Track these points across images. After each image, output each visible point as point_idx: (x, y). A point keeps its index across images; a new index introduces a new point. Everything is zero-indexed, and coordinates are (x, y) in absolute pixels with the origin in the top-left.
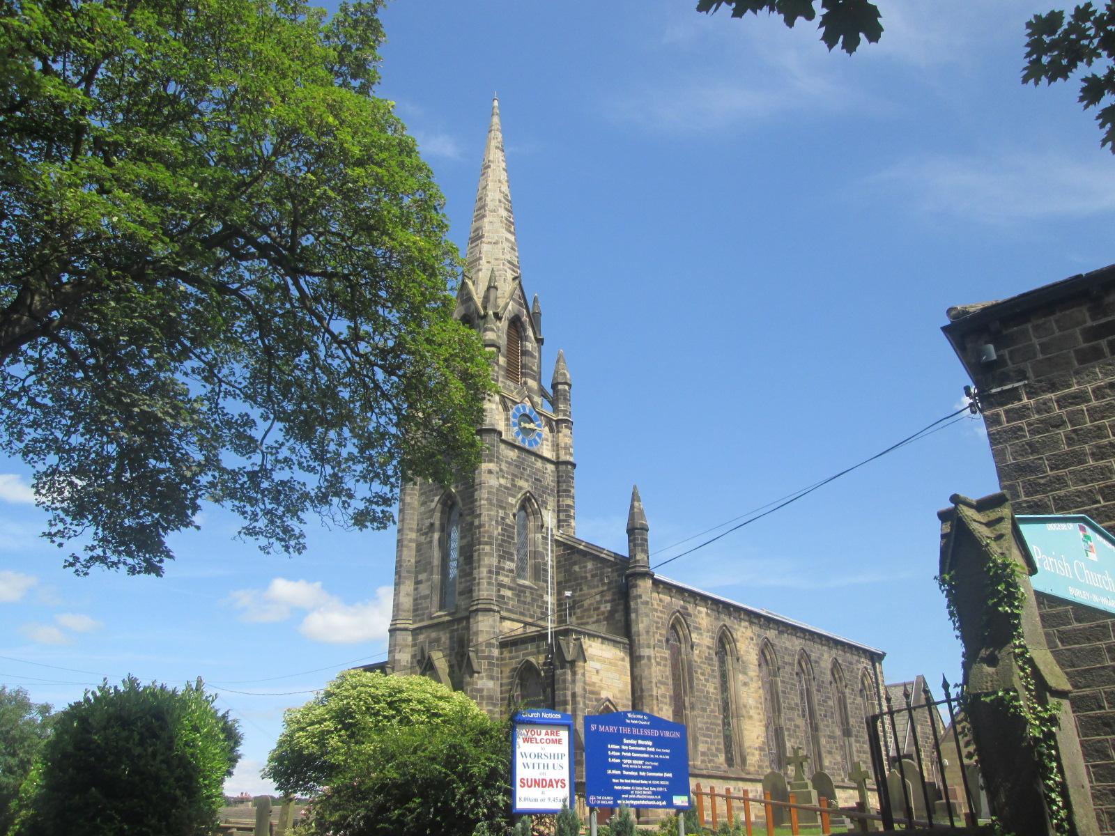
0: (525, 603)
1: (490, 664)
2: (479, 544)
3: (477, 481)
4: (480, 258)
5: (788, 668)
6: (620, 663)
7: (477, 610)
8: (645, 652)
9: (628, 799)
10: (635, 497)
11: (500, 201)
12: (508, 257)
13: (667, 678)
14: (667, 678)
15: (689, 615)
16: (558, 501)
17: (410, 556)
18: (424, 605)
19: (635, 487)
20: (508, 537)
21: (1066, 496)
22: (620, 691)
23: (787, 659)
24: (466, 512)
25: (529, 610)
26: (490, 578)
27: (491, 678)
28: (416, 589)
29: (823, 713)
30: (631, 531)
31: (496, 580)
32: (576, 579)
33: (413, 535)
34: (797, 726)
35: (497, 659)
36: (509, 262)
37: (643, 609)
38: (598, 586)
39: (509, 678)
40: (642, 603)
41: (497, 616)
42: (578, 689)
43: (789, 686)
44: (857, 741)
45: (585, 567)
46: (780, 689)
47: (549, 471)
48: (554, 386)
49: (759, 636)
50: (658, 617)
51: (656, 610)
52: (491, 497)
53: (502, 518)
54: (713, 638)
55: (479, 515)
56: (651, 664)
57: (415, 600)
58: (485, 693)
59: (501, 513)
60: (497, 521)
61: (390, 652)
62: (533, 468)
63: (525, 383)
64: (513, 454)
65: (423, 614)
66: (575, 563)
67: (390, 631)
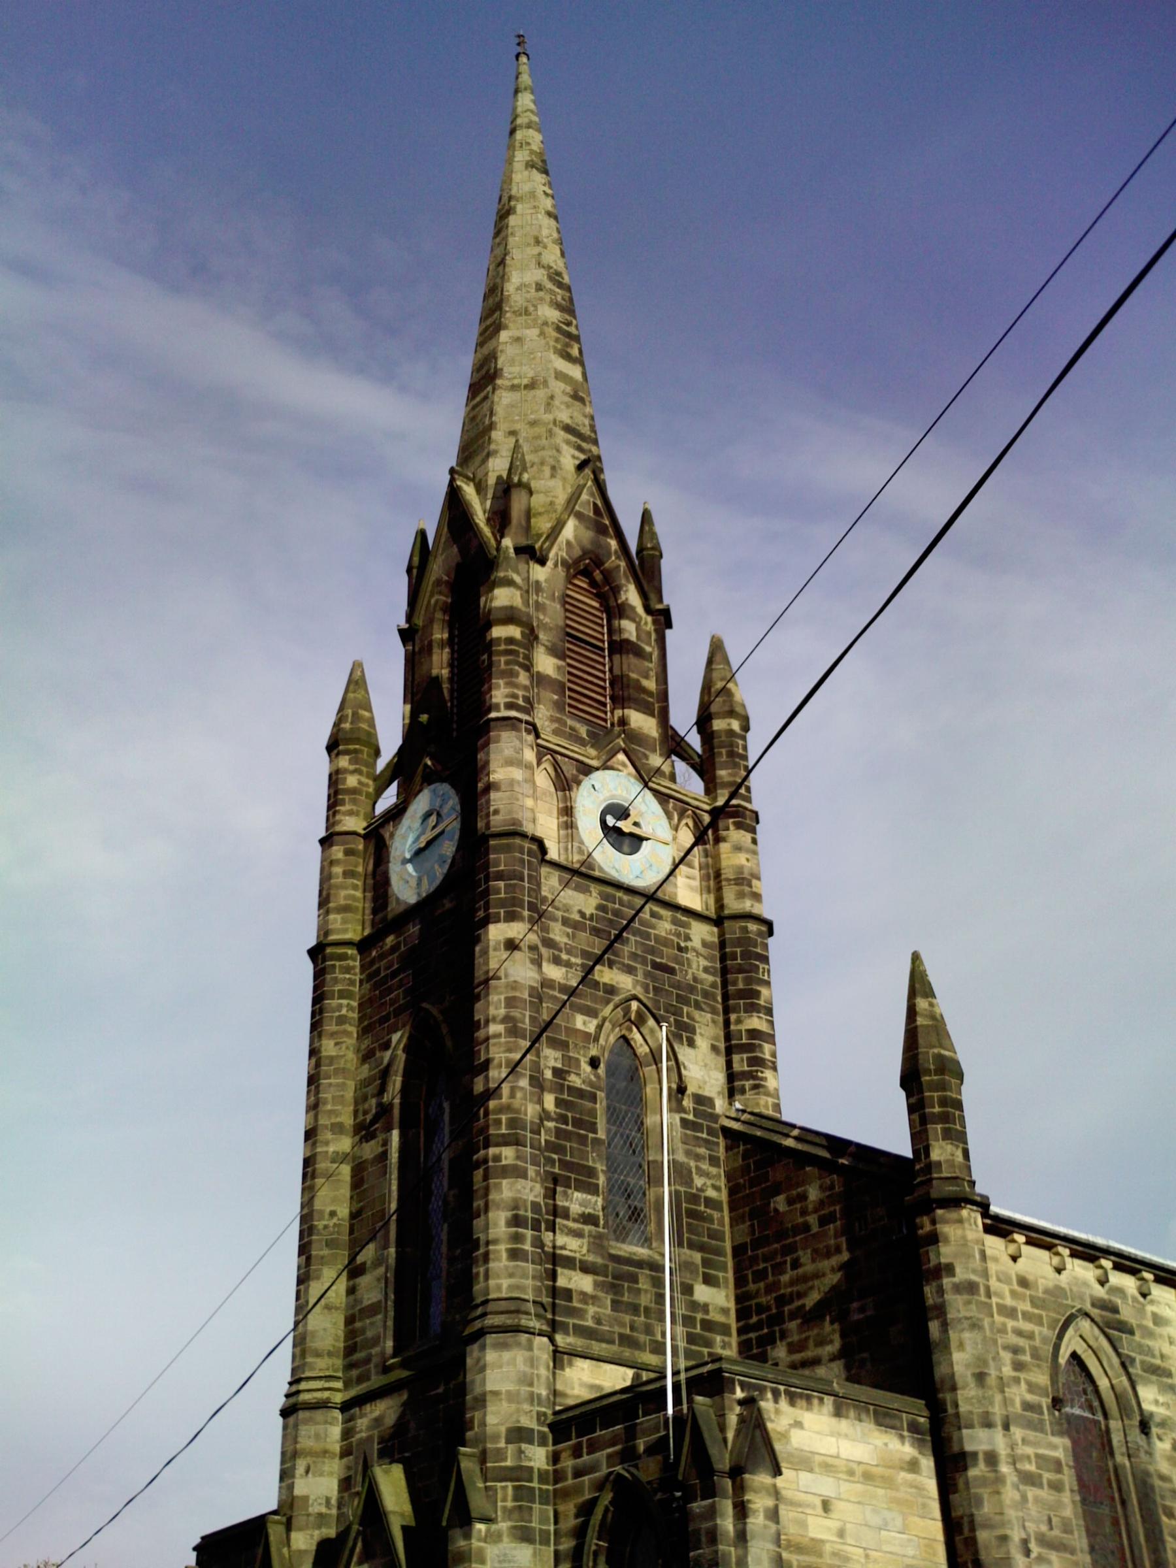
0: (635, 1309)
1: (521, 1494)
3: (479, 975)
4: (491, 426)
6: (904, 1476)
7: (481, 1333)
8: (976, 1440)
10: (919, 985)
12: (564, 416)
13: (1067, 1528)
14: (1067, 1528)
15: (1125, 1328)
18: (370, 1334)
19: (916, 957)
20: (578, 1123)
26: (517, 1238)
27: (524, 1535)
28: (351, 1291)
30: (911, 1079)
31: (538, 1243)
33: (345, 1144)
36: (568, 429)
37: (958, 1307)
40: (958, 1289)
45: (803, 1197)
47: (696, 943)
48: (703, 722)
50: (1019, 1333)
51: (1011, 1313)
52: (516, 1013)
53: (557, 1072)
56: (1000, 1480)
57: (350, 1321)
62: (647, 936)
63: (623, 722)
67: (285, 1413)
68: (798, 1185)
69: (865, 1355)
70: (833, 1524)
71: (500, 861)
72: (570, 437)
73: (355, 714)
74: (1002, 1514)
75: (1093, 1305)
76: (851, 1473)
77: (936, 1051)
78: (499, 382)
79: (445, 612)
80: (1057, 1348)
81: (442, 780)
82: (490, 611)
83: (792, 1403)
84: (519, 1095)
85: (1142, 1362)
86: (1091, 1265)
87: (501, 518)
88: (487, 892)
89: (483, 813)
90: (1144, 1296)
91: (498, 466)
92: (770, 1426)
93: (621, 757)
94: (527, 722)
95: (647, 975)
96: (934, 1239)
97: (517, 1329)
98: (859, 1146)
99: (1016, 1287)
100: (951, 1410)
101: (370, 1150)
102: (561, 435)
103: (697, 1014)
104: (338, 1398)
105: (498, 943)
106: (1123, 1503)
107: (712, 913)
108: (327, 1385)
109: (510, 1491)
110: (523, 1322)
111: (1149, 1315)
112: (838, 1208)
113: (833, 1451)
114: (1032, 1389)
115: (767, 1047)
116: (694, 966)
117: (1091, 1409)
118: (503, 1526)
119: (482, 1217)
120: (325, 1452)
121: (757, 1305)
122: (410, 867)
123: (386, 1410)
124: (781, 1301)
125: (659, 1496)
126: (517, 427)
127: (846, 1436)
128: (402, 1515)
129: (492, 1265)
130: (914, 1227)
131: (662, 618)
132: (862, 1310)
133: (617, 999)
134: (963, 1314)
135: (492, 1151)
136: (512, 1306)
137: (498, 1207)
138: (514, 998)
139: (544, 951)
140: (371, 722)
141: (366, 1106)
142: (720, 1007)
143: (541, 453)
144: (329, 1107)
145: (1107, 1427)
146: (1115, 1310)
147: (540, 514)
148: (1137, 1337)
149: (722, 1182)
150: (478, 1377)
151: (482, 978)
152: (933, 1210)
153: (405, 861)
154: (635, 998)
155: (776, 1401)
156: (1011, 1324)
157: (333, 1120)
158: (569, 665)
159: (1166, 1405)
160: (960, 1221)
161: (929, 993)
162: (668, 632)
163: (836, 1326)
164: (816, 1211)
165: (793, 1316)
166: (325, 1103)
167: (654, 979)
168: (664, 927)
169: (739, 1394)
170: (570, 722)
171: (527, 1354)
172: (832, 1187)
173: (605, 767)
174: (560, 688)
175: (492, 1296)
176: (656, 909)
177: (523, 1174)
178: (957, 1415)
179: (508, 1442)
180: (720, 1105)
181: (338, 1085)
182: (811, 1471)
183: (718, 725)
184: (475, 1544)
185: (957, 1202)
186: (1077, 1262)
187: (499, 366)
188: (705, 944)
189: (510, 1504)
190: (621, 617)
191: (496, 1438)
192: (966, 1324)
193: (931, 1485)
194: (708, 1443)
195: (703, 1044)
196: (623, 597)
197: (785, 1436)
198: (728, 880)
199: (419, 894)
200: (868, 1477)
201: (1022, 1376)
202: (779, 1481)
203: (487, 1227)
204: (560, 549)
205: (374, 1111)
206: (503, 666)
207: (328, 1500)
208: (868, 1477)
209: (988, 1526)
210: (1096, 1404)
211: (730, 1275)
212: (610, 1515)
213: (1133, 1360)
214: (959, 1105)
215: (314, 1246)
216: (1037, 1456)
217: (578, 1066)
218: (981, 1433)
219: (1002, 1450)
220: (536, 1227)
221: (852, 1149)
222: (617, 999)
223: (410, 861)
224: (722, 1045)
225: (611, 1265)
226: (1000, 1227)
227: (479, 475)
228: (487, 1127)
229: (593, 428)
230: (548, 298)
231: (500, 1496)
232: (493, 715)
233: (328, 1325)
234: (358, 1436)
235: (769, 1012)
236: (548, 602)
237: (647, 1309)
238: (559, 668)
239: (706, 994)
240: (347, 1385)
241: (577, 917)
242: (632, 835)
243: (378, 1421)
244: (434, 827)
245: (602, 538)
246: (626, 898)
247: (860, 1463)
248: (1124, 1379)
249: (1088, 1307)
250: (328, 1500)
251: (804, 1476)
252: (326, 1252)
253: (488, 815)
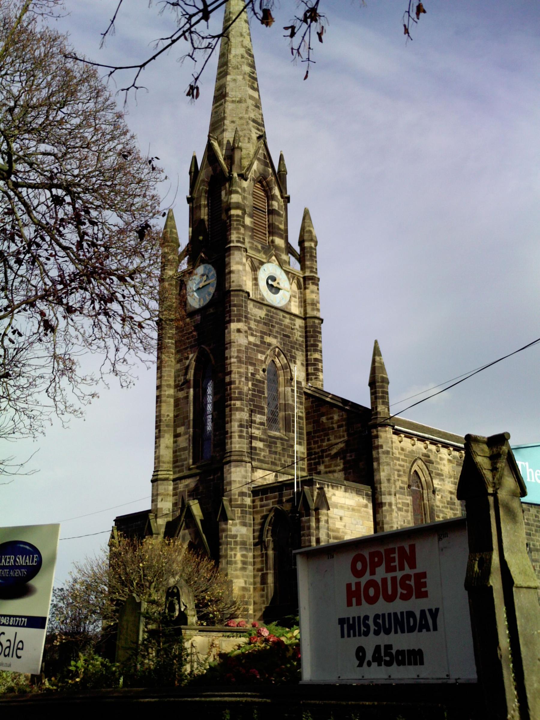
1: (243, 512)
2: (231, 400)
3: (227, 340)
4: (224, 118)
7: (230, 462)
8: (386, 499)
10: (376, 352)
11: (243, 57)
12: (252, 115)
15: (431, 462)
17: (169, 411)
18: (183, 457)
19: (376, 342)
20: (259, 391)
25: (280, 460)
26: (241, 431)
27: (244, 524)
28: (175, 442)
30: (372, 384)
31: (247, 433)
32: (324, 430)
33: (171, 391)
35: (250, 507)
36: (254, 121)
37: (383, 458)
40: (384, 453)
43: (534, 528)
45: (332, 418)
47: (297, 327)
48: (301, 242)
50: (400, 465)
51: (398, 459)
52: (240, 355)
53: (252, 374)
54: (455, 484)
55: (230, 373)
56: (392, 510)
57: (175, 452)
59: (251, 369)
60: (247, 379)
61: (153, 501)
62: (281, 325)
63: (273, 242)
65: (182, 465)
66: (323, 415)
67: (153, 481)
68: (330, 414)
69: (351, 471)
70: (343, 524)
71: (235, 300)
72: (255, 124)
73: (171, 231)
74: (392, 520)
75: (422, 455)
76: (348, 509)
77: (381, 375)
78: (227, 98)
79: (206, 193)
80: (411, 469)
81: (209, 263)
82: (230, 203)
83: (333, 488)
84: (242, 383)
85: (435, 472)
86: (422, 443)
87: (230, 158)
88: (230, 311)
89: (228, 281)
90: (438, 451)
91: (228, 136)
92: (327, 495)
93: (274, 258)
94: (244, 248)
95: (281, 339)
96: (377, 437)
97: (242, 461)
98: (352, 403)
99: (400, 451)
100: (379, 490)
101: (181, 395)
102: (251, 123)
103: (297, 352)
104: (171, 477)
105: (234, 330)
106: (425, 514)
107: (302, 315)
108: (168, 473)
109: (239, 511)
110: (244, 459)
111: (439, 458)
112: (344, 423)
113: (344, 503)
114: (403, 482)
115: (320, 364)
116: (296, 335)
117: (418, 487)
118: (237, 521)
119: (229, 424)
120: (168, 494)
121: (315, 452)
122: (195, 294)
123: (191, 483)
124: (323, 451)
125: (290, 515)
126: (234, 119)
127: (348, 498)
128: (199, 516)
129: (233, 440)
130: (371, 433)
131: (287, 200)
132: (351, 456)
133: (271, 348)
134: (385, 460)
135: (233, 402)
136: (240, 453)
137: (235, 421)
138: (240, 350)
139: (249, 332)
140: (176, 234)
141: (179, 379)
142: (304, 349)
143: (244, 132)
144: (166, 378)
145: (423, 492)
146: (429, 457)
147: (244, 158)
148: (434, 465)
149: (303, 411)
150: (229, 476)
151: (229, 342)
152: (377, 428)
153: (193, 291)
154: (277, 347)
155: (328, 488)
156: (398, 462)
157: (168, 383)
158: (255, 220)
159: (441, 485)
160: (386, 431)
161: (380, 355)
162: (288, 204)
163: (342, 461)
164: (336, 423)
165: (327, 456)
166: (164, 377)
167: (283, 340)
168: (287, 321)
169: (318, 486)
170: (255, 243)
171: (245, 469)
172: (342, 416)
173: (268, 262)
174: (252, 230)
175: (233, 450)
178: (381, 491)
179: (239, 496)
180: (304, 384)
181: (169, 371)
182: (337, 508)
183: (307, 244)
184: (229, 526)
185: (385, 425)
186: (419, 442)
187: (227, 91)
188: (300, 327)
189: (239, 515)
190: (272, 200)
191: (235, 495)
192: (385, 464)
193: (371, 512)
194: (308, 500)
196: (274, 192)
197: (330, 498)
198: (309, 303)
199: (200, 305)
200: (353, 510)
201: (400, 478)
202: (329, 512)
203: (231, 427)
204: (252, 174)
205: (183, 381)
206: (235, 226)
207: (169, 509)
208: (353, 510)
209: (388, 523)
210: (420, 485)
211: (305, 442)
212: (273, 520)
213: (432, 472)
214: (387, 393)
215: (161, 426)
216: (402, 502)
217: (259, 372)
218: (388, 497)
219: (393, 502)
220: (247, 428)
221: (350, 404)
222: (271, 348)
223: (195, 291)
224: (305, 363)
225: (269, 439)
226: (397, 432)
227: (220, 138)
228: (231, 394)
229: (262, 119)
230: (246, 61)
231: (236, 512)
232: (232, 245)
233: (167, 453)
234: (179, 490)
235: (321, 352)
236: (247, 196)
237: (279, 453)
238: (251, 222)
239: (300, 345)
240: (174, 473)
241: (259, 319)
242: (276, 287)
243: (187, 486)
244: (205, 281)
245: (266, 168)
246: (275, 311)
247: (351, 506)
248: (429, 478)
249: (421, 456)
250: (169, 509)
251: (335, 510)
252: (166, 428)
253: (230, 282)
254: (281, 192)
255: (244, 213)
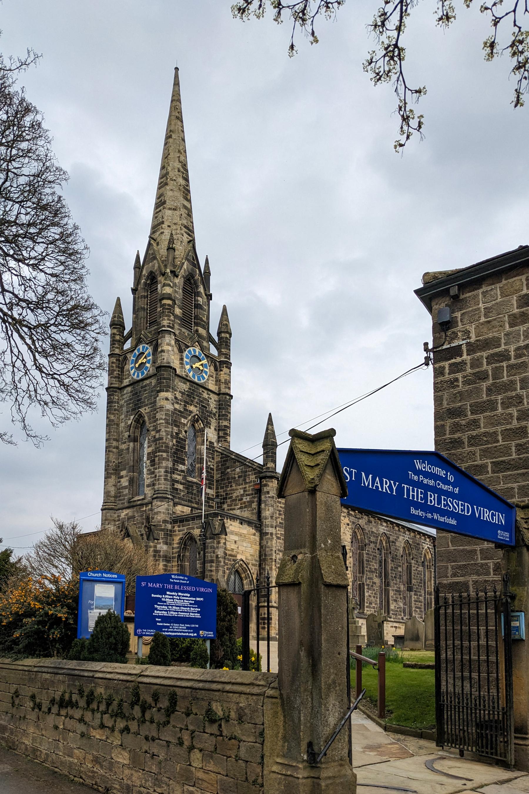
4: (163, 223)
5: (372, 545)
9: (167, 632)
16: (219, 422)
20: (181, 447)
21: (477, 435)
22: (251, 555)
23: (372, 539)
24: (151, 428)
25: (195, 499)
26: (166, 476)
29: (393, 575)
30: (265, 446)
31: (171, 477)
32: (228, 479)
34: (375, 583)
36: (185, 227)
38: (242, 484)
39: (177, 544)
41: (171, 503)
42: (220, 552)
44: (415, 595)
46: (365, 558)
48: (219, 334)
49: (353, 523)
56: (273, 538)
58: (161, 554)
59: (176, 430)
63: (197, 331)
64: (184, 387)
70: (237, 546)
93: (197, 343)
95: (200, 408)
136: (165, 492)
154: (197, 415)
156: (279, 505)
160: (272, 482)
161: (272, 425)
168: (205, 395)
176: (203, 390)
177: (168, 460)
193: (258, 539)
195: (213, 428)
197: (228, 528)
224: (217, 428)
235: (230, 421)
254: (205, 290)
255: (174, 301)
